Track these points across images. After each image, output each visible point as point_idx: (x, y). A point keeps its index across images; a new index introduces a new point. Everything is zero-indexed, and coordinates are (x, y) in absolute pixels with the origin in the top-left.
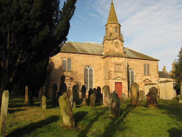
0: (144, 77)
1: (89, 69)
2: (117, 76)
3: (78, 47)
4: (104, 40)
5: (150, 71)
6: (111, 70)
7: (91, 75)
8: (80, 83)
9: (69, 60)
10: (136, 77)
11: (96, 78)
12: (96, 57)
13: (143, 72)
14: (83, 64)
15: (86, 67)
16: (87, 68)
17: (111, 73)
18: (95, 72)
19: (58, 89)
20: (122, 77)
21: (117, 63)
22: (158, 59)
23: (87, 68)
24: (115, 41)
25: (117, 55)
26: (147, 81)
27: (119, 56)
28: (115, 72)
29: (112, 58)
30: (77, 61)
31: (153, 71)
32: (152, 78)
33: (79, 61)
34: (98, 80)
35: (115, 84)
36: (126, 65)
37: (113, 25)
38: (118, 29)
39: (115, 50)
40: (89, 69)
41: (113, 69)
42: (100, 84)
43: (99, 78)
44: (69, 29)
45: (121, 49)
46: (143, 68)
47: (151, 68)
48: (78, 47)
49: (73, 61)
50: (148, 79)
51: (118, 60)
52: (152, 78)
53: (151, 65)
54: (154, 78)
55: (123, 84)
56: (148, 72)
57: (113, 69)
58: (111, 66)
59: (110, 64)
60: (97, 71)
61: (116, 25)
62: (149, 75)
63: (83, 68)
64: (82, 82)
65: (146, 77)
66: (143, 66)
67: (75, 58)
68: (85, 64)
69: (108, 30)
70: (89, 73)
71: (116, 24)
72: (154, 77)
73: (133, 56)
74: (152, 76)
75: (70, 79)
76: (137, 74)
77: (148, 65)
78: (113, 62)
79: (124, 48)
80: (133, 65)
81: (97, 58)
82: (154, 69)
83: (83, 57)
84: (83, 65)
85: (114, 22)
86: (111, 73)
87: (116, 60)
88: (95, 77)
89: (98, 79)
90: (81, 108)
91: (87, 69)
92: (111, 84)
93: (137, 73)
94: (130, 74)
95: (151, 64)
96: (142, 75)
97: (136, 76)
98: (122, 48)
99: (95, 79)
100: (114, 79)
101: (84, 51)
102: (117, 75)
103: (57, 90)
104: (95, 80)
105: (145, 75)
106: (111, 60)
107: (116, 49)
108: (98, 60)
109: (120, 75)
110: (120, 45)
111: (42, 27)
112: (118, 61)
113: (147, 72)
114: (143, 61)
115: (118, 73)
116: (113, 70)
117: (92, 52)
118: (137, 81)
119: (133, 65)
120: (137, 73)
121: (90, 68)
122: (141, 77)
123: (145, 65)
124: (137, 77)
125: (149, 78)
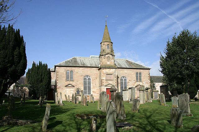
0: (136, 83)
1: (87, 78)
3: (81, 62)
4: (100, 55)
5: (142, 78)
6: (103, 79)
7: (89, 83)
8: (80, 89)
9: (72, 71)
11: (93, 85)
12: (93, 68)
13: (135, 79)
16: (86, 77)
18: (93, 80)
22: (150, 68)
23: (86, 77)
24: (107, 56)
25: (108, 67)
26: (70, 86)
27: (110, 67)
32: (143, 84)
33: (79, 73)
34: (95, 87)
37: (106, 43)
38: (110, 46)
39: (107, 63)
40: (87, 78)
41: (104, 78)
42: (97, 90)
44: (27, 65)
47: (143, 75)
50: (139, 85)
56: (140, 79)
57: (104, 78)
58: (103, 76)
59: (102, 74)
60: (95, 80)
61: (108, 43)
62: (140, 80)
63: (83, 78)
65: (138, 83)
66: (135, 74)
67: (76, 70)
68: (84, 75)
69: (102, 48)
74: (144, 82)
76: (129, 81)
77: (140, 73)
79: (115, 61)
81: (94, 70)
85: (107, 41)
87: (108, 71)
88: (93, 84)
89: (95, 86)
93: (130, 80)
95: (143, 72)
96: (135, 81)
97: (129, 82)
98: (113, 61)
99: (93, 86)
101: (84, 64)
105: (137, 81)
108: (95, 70)
109: (110, 82)
111: (11, 66)
113: (139, 78)
115: (108, 81)
120: (130, 80)
121: (88, 77)
122: (133, 83)
124: (130, 84)
125: (141, 84)
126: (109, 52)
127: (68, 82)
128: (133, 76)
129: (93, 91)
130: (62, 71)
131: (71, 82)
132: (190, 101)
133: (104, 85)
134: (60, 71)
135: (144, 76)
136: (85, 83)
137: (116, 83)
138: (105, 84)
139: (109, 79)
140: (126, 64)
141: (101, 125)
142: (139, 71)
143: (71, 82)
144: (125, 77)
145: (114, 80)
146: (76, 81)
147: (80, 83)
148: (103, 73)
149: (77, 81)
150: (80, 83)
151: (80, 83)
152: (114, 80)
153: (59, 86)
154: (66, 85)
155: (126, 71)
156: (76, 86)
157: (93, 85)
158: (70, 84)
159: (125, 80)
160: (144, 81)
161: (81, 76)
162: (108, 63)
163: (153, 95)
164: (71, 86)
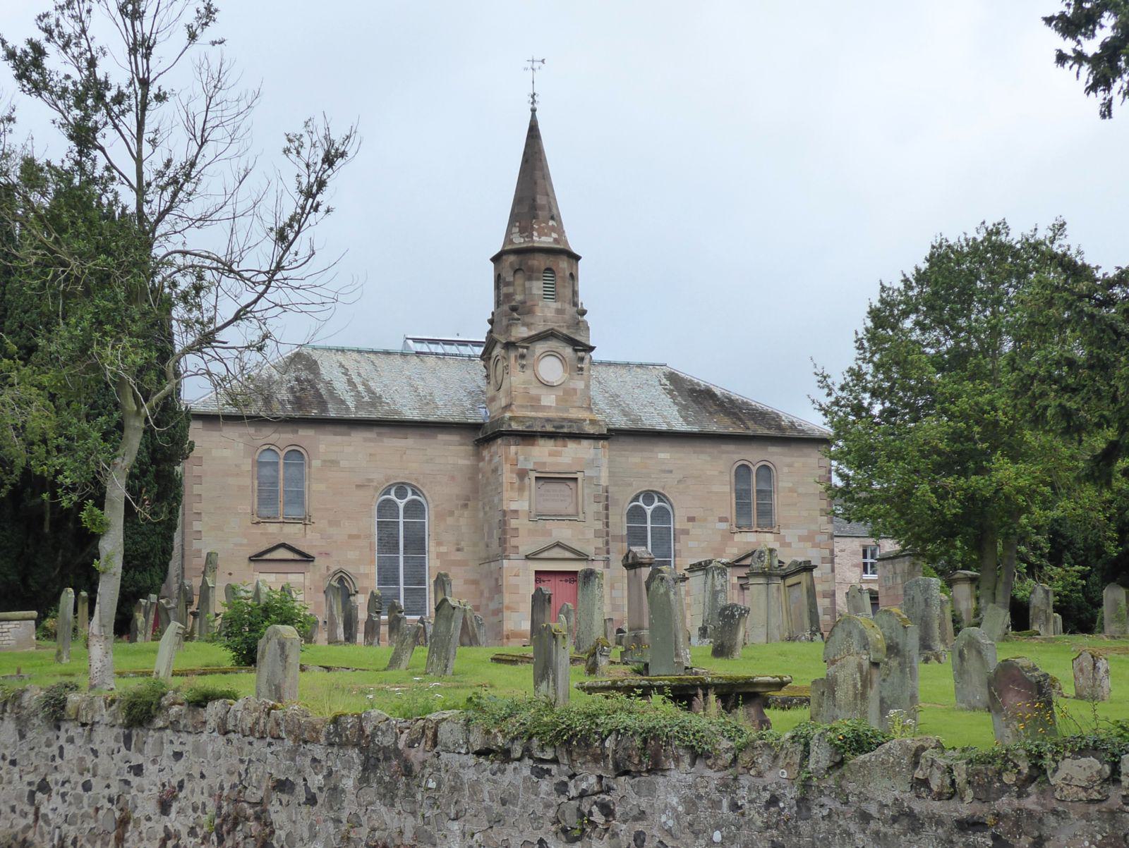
0: (737, 537)
1: (401, 504)
2: (544, 542)
3: (350, 382)
5: (778, 501)
6: (514, 506)
11: (443, 549)
15: (388, 492)
19: (196, 600)
25: (549, 428)
28: (541, 516)
33: (343, 463)
36: (598, 478)
40: (401, 504)
43: (458, 550)
45: (575, 390)
46: (727, 489)
47: (783, 482)
48: (350, 382)
49: (316, 463)
53: (786, 470)
54: (802, 545)
65: (748, 540)
72: (801, 539)
73: (669, 416)
75: (297, 557)
82: (801, 490)
83: (365, 440)
84: (370, 480)
87: (543, 454)
88: (439, 544)
90: (345, 705)
92: (513, 580)
93: (691, 519)
95: (788, 460)
96: (724, 526)
97: (686, 532)
99: (439, 555)
103: (191, 603)
114: (731, 447)
115: (550, 525)
116: (527, 508)
117: (427, 401)
120: (691, 519)
121: (410, 497)
123: (743, 471)
127: (272, 528)
135: (792, 490)
137: (597, 534)
142: (754, 456)
144: (662, 497)
155: (664, 455)
160: (787, 527)
161: (358, 486)
164: (290, 555)
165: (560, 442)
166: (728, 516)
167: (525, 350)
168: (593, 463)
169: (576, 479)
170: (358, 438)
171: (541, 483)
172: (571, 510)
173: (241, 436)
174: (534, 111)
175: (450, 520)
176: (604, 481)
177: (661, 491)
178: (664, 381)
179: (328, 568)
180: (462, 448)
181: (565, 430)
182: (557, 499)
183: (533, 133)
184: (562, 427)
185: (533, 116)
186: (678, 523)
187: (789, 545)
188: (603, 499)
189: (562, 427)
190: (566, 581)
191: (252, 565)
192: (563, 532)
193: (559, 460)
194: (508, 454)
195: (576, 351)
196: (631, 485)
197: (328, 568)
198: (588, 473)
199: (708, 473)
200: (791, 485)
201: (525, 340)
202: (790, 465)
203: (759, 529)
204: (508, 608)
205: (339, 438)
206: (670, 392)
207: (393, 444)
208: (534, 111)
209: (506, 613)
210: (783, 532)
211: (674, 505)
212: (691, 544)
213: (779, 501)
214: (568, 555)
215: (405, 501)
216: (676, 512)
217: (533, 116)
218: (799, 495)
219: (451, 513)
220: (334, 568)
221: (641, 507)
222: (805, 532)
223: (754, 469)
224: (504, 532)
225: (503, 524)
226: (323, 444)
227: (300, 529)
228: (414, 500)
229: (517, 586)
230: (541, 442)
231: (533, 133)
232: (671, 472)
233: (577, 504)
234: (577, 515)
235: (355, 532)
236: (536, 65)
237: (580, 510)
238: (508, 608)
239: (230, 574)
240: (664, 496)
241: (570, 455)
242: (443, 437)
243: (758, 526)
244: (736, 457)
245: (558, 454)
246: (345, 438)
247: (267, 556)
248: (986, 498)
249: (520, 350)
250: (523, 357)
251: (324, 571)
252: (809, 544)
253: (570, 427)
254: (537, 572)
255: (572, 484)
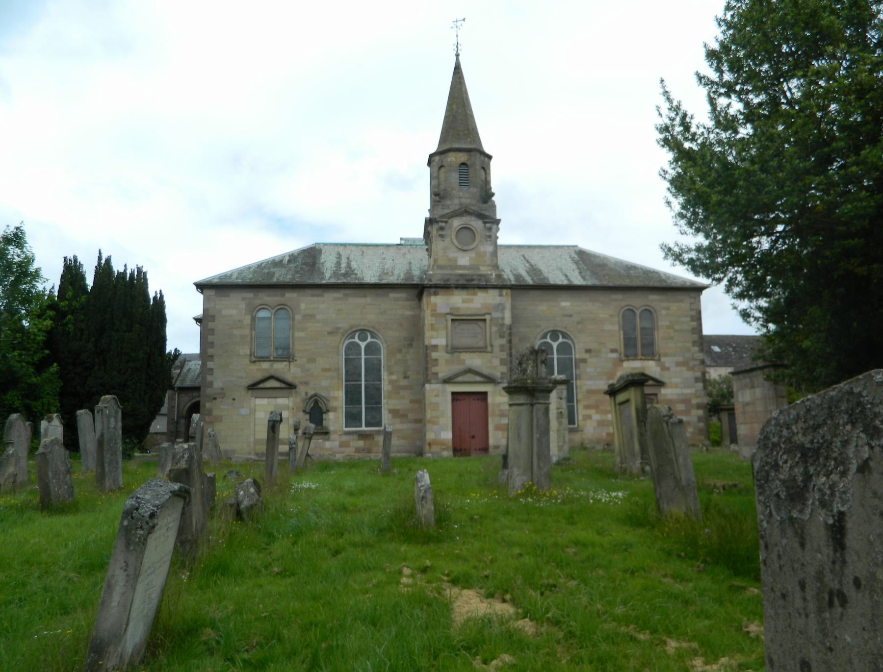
0: (626, 364)
1: (363, 345)
2: (457, 368)
6: (434, 342)
7: (374, 370)
9: (648, 312)
10: (582, 365)
11: (394, 377)
14: (340, 325)
17: (434, 355)
20: (485, 371)
21: (461, 313)
29: (436, 294)
30: (310, 317)
31: (672, 338)
32: (664, 368)
33: (319, 317)
35: (453, 400)
36: (503, 318)
39: (455, 260)
40: (363, 345)
43: (405, 378)
45: (485, 252)
46: (616, 327)
51: (464, 301)
52: (664, 368)
53: (664, 312)
54: (679, 369)
55: (490, 400)
58: (433, 327)
59: (429, 320)
61: (462, 157)
62: (649, 351)
64: (336, 398)
68: (344, 325)
70: (558, 359)
71: (461, 154)
72: (678, 364)
74: (667, 361)
75: (283, 385)
76: (586, 356)
78: (442, 309)
80: (566, 316)
82: (677, 327)
83: (335, 299)
84: (338, 329)
86: (434, 355)
87: (458, 300)
91: (359, 346)
92: (434, 400)
93: (588, 351)
94: (555, 356)
95: (665, 305)
96: (615, 355)
97: (584, 361)
99: (391, 382)
100: (447, 381)
102: (462, 362)
104: (390, 388)
105: (628, 357)
106: (435, 305)
107: (459, 255)
110: (478, 238)
112: (465, 305)
114: (618, 296)
115: (464, 356)
118: (588, 382)
119: (566, 316)
120: (588, 351)
126: (468, 201)
127: (265, 365)
128: (608, 327)
129: (390, 411)
130: (233, 312)
131: (280, 368)
132: (492, 352)
133: (442, 375)
134: (224, 312)
135: (668, 327)
136: (352, 374)
137: (503, 362)
138: (443, 370)
139: (467, 341)
140: (574, 267)
141: (784, 480)
142: (638, 302)
143: (280, 368)
144: (565, 335)
145: (496, 349)
146: (305, 360)
147: (328, 370)
148: (434, 314)
149: (312, 360)
150: (324, 370)
151: (328, 370)
152: (496, 349)
153: (221, 385)
154: (251, 381)
155: (566, 303)
156: (306, 383)
157: (394, 377)
158: (273, 373)
159: (565, 349)
160: (666, 355)
161: (329, 333)
162: (464, 260)
163: (730, 424)
164: (276, 384)
165: (471, 291)
166: (618, 347)
167: (444, 224)
168: (500, 307)
169: (485, 320)
170: (330, 296)
171: (457, 323)
172: (481, 344)
173: (243, 299)
174: (457, 55)
175: (399, 356)
176: (508, 321)
177: (564, 330)
178: (574, 255)
179: (306, 394)
180: (408, 303)
181: (475, 282)
182: (467, 335)
183: (458, 70)
184: (473, 280)
185: (457, 60)
186: (578, 354)
187: (668, 369)
188: (506, 335)
189: (473, 280)
190: (478, 399)
191: (250, 392)
192: (475, 361)
193: (471, 305)
194: (439, 302)
195: (485, 223)
196: (539, 326)
197: (306, 394)
198: (496, 315)
199: (601, 316)
200: (668, 323)
201: (442, 216)
202: (667, 309)
203: (643, 358)
204: (430, 421)
205: (315, 299)
206: (577, 263)
207: (357, 302)
208: (457, 55)
209: (428, 426)
210: (663, 359)
211: (575, 341)
212: (588, 370)
213: (660, 336)
214: (478, 379)
215: (365, 343)
216: (577, 346)
217: (457, 60)
218: (675, 331)
219: (400, 351)
220: (311, 393)
221: (548, 343)
222: (681, 359)
223: (638, 312)
224: (427, 362)
225: (427, 355)
226: (305, 303)
227: (286, 366)
228: (371, 342)
229: (437, 404)
230: (456, 292)
231: (458, 70)
232: (571, 316)
233: (486, 340)
234: (486, 347)
235: (327, 366)
236: (459, 24)
237: (488, 341)
238: (430, 421)
239: (234, 399)
240: (566, 334)
241: (480, 301)
242: (393, 295)
243: (642, 355)
244: (623, 303)
245: (471, 301)
246: (320, 299)
247: (261, 386)
248: (861, 150)
249: (440, 224)
250: (442, 229)
251: (303, 395)
252: (684, 369)
253: (480, 280)
254: (453, 394)
255: (481, 323)
